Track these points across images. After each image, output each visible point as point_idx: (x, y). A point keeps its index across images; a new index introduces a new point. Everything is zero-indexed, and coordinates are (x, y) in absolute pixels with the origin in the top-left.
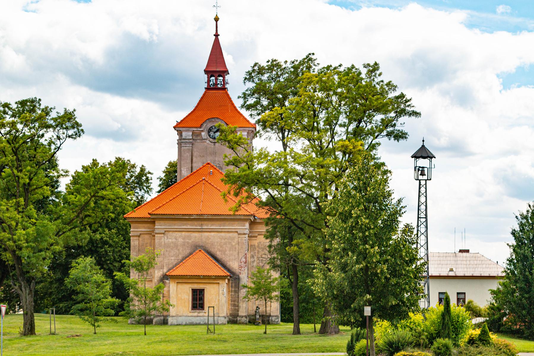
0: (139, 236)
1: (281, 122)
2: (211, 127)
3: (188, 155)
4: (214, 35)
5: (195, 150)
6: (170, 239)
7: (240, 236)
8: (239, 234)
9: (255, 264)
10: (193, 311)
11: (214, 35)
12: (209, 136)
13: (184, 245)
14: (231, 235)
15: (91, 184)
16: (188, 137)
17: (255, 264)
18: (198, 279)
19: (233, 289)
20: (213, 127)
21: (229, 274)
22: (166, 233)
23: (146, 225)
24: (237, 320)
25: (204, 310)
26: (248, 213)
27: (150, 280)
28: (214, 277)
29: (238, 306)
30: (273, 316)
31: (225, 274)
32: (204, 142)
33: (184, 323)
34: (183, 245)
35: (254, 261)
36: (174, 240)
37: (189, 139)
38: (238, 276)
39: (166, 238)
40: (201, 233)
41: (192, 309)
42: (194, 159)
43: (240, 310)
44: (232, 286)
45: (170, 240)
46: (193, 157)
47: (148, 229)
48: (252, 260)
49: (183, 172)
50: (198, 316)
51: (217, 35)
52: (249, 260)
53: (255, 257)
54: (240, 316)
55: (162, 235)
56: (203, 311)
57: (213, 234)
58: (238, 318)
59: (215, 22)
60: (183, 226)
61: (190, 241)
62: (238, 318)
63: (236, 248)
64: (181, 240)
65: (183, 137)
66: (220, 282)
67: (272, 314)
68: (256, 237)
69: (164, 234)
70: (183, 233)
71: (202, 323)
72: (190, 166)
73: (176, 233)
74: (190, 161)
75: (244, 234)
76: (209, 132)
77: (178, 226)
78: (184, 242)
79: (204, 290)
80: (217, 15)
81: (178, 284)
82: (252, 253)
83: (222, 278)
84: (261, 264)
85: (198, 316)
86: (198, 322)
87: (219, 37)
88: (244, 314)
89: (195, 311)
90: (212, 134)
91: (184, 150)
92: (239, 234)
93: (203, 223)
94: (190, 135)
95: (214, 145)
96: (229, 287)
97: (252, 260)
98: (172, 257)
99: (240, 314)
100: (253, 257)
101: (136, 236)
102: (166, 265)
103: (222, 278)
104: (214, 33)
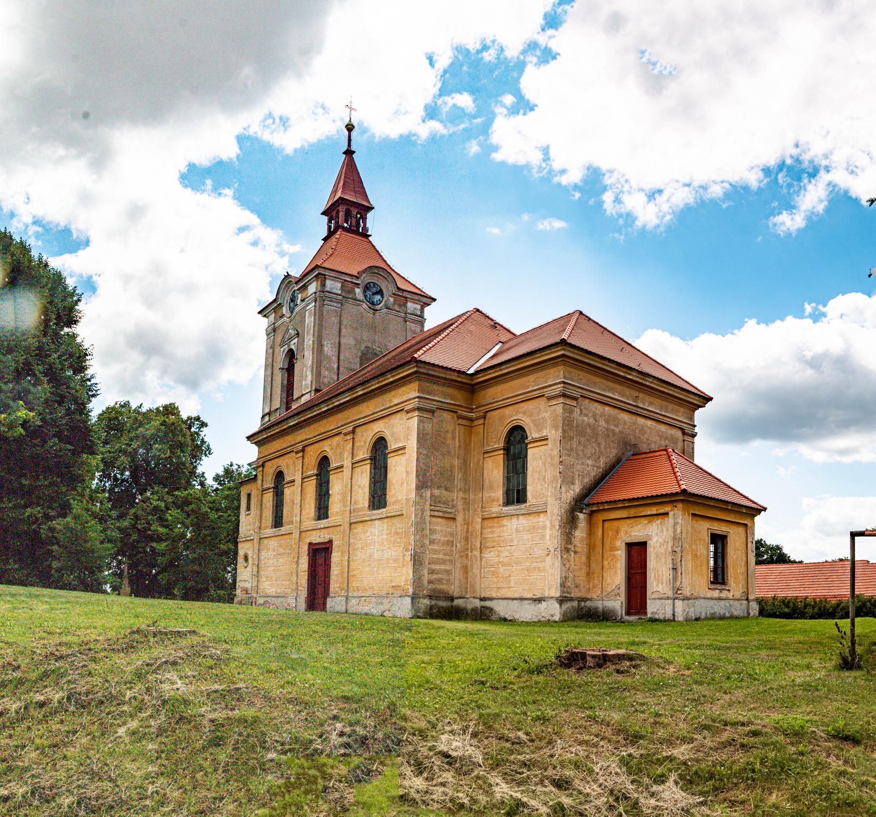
0: (353, 432)
2: (369, 283)
3: (334, 320)
4: (354, 152)
5: (344, 315)
6: (586, 415)
11: (354, 152)
12: (365, 296)
13: (608, 436)
16: (334, 291)
20: (372, 284)
23: (451, 391)
27: (451, 516)
32: (359, 305)
33: (703, 616)
34: (608, 434)
36: (592, 420)
37: (337, 294)
40: (634, 417)
41: (306, 610)
42: (343, 331)
45: (585, 419)
46: (342, 327)
47: (451, 399)
49: (326, 349)
50: (720, 599)
51: (349, 153)
57: (649, 423)
59: (347, 133)
60: (609, 392)
65: (328, 288)
70: (607, 408)
72: (337, 342)
73: (596, 404)
74: (336, 332)
77: (600, 388)
78: (608, 429)
79: (726, 537)
80: (350, 121)
85: (720, 599)
87: (354, 156)
90: (369, 293)
91: (328, 311)
94: (339, 288)
95: (374, 314)
98: (589, 458)
102: (579, 475)
104: (345, 148)
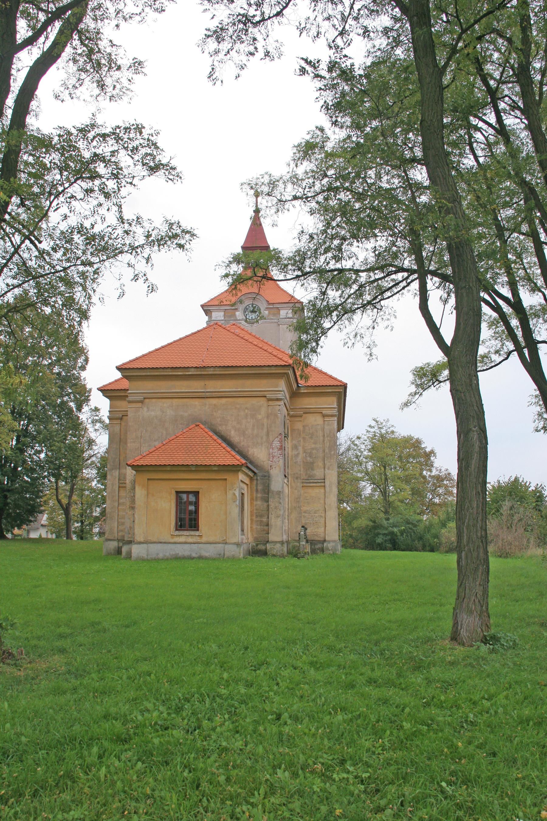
1: (289, 722)
7: (271, 403)
8: (269, 400)
9: (300, 458)
10: (177, 533)
14: (254, 401)
15: (304, 509)
17: (300, 458)
18: (184, 471)
19: (259, 495)
21: (244, 461)
22: (147, 400)
24: (266, 549)
25: (198, 530)
26: (283, 363)
28: (216, 469)
29: (268, 525)
30: (329, 542)
31: (237, 463)
35: (298, 454)
38: (268, 472)
39: (145, 409)
43: (272, 531)
44: (257, 491)
45: (153, 413)
48: (295, 452)
50: (186, 543)
52: (290, 453)
53: (300, 449)
54: (272, 542)
55: (139, 405)
56: (197, 533)
57: (224, 401)
58: (269, 546)
61: (186, 414)
62: (269, 546)
63: (263, 425)
64: (170, 412)
65: (213, 319)
66: (229, 477)
67: (327, 538)
68: (301, 416)
69: (142, 402)
71: (194, 555)
75: (278, 400)
76: (245, 312)
81: (150, 482)
82: (294, 442)
83: (234, 469)
84: (308, 459)
86: (187, 553)
88: (279, 539)
89: (181, 533)
92: (269, 400)
93: (207, 382)
96: (252, 492)
97: (295, 452)
98: (155, 441)
99: (272, 538)
100: (295, 447)
101: (117, 419)
103: (234, 469)
